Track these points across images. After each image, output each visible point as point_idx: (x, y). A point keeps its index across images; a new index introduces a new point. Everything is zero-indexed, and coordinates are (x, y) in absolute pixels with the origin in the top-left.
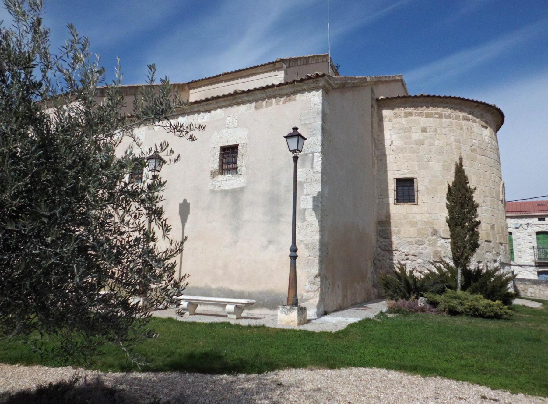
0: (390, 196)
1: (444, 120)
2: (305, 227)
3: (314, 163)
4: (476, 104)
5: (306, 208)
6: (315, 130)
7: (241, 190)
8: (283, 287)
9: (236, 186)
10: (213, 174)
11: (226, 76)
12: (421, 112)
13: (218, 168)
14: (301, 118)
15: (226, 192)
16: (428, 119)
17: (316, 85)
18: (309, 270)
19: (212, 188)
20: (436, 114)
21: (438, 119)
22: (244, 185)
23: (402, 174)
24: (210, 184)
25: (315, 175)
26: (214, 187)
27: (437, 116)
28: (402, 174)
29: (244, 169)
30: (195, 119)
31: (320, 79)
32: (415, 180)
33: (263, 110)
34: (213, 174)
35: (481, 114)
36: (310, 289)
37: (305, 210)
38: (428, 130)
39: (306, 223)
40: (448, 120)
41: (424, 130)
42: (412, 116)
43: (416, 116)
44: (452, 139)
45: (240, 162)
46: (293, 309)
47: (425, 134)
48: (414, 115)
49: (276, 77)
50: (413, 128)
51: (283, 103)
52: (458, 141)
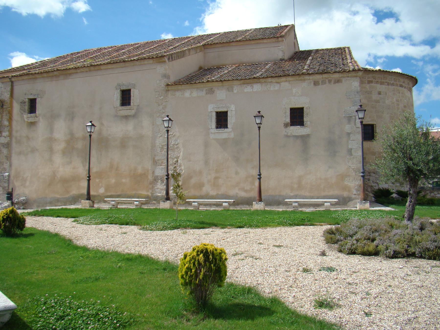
0: (20, 72)
1: (390, 87)
2: (352, 158)
3: (356, 122)
4: (407, 77)
5: (352, 148)
6: (356, 102)
7: (308, 136)
8: (85, 191)
9: (304, 134)
10: (286, 125)
11: (237, 42)
12: (378, 81)
13: (289, 122)
14: (347, 94)
15: (297, 137)
16: (382, 85)
17: (356, 75)
18: (355, 183)
19: (286, 134)
20: (386, 82)
21: (387, 86)
22: (310, 133)
23: (367, 122)
24: (284, 131)
25: (357, 129)
26: (288, 133)
27: (386, 84)
28: (367, 122)
29: (309, 123)
30: (268, 87)
31: (360, 72)
32: (375, 126)
33: (319, 86)
34: (286, 125)
35: (408, 83)
36: (356, 193)
37: (351, 149)
38: (382, 93)
39: (353, 157)
40: (393, 87)
41: (379, 93)
42: (372, 83)
43: (374, 83)
44: (395, 100)
45: (305, 119)
46: (367, 202)
47: (380, 96)
48: (374, 83)
49: (279, 47)
50: (373, 91)
51: (333, 84)
52: (397, 101)
